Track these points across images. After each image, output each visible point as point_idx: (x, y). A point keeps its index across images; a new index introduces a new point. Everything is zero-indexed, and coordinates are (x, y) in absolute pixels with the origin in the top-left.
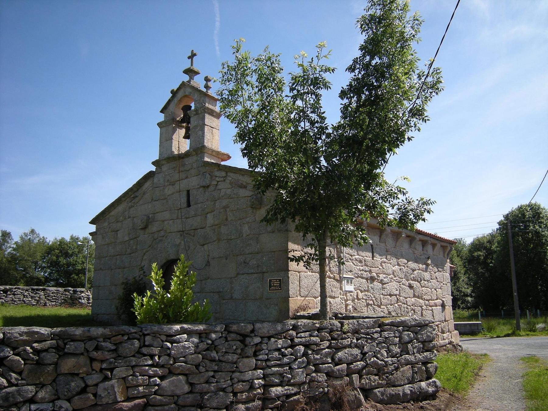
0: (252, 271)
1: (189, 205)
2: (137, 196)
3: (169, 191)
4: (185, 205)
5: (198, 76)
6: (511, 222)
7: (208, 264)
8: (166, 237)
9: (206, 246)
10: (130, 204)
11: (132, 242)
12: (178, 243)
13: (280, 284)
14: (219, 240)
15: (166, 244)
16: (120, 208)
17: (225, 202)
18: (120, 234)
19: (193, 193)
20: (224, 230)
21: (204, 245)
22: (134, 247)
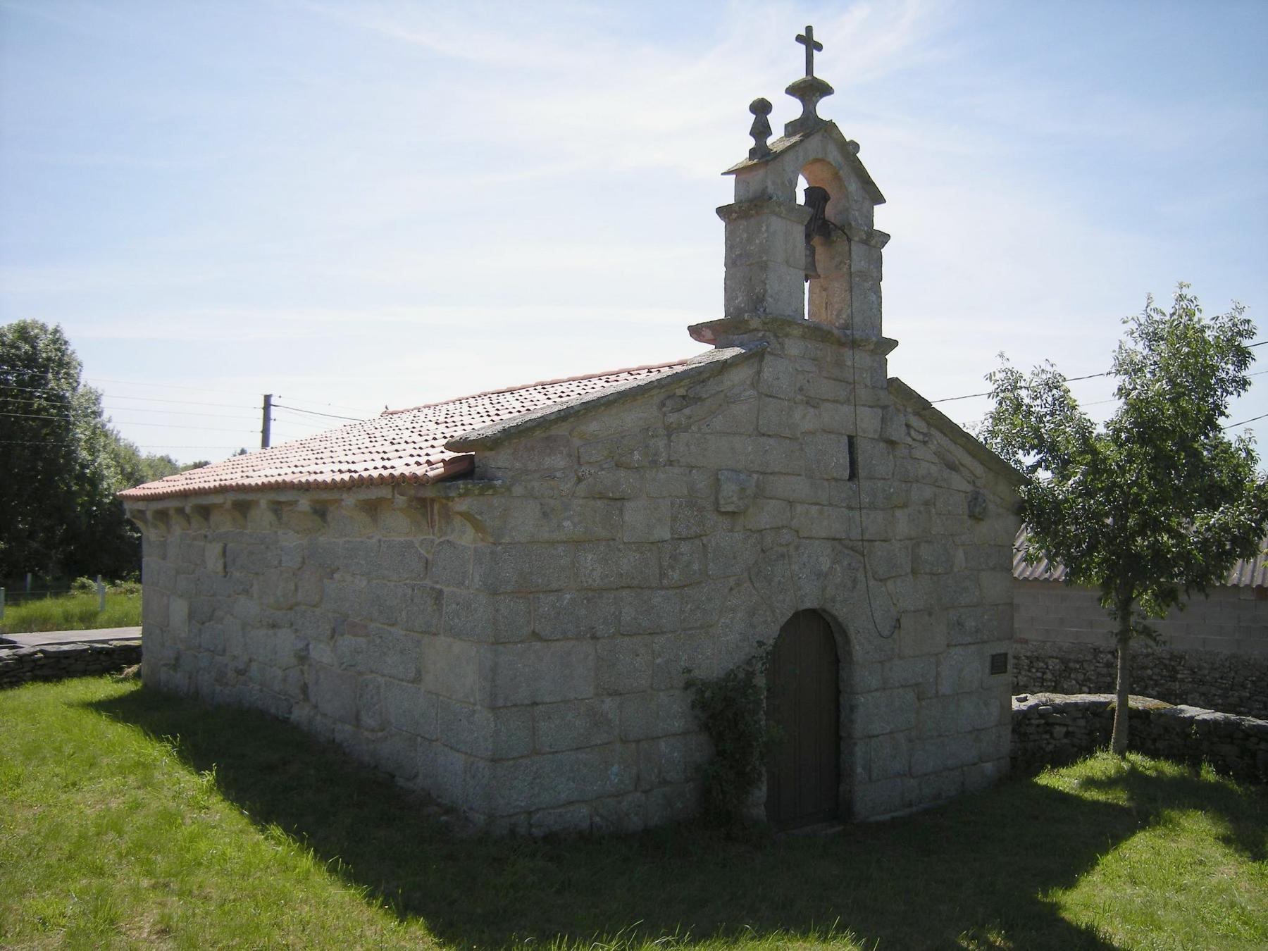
0: (969, 639)
1: (853, 475)
2: (700, 399)
3: (805, 420)
4: (846, 475)
5: (790, 82)
6: (104, 426)
7: (898, 625)
8: (797, 548)
9: (890, 584)
10: (673, 418)
11: (684, 547)
12: (825, 568)
13: (616, 693)
14: (914, 572)
15: (796, 567)
16: (631, 419)
17: (928, 492)
18: (634, 516)
19: (863, 446)
20: (925, 552)
21: (886, 579)
22: (696, 567)
